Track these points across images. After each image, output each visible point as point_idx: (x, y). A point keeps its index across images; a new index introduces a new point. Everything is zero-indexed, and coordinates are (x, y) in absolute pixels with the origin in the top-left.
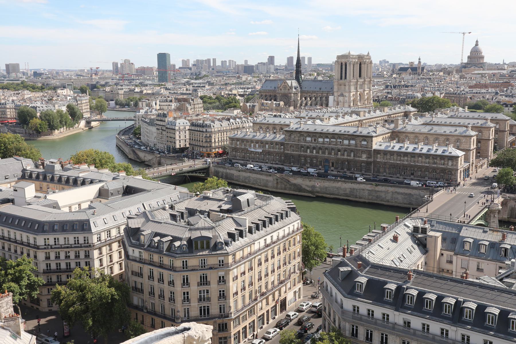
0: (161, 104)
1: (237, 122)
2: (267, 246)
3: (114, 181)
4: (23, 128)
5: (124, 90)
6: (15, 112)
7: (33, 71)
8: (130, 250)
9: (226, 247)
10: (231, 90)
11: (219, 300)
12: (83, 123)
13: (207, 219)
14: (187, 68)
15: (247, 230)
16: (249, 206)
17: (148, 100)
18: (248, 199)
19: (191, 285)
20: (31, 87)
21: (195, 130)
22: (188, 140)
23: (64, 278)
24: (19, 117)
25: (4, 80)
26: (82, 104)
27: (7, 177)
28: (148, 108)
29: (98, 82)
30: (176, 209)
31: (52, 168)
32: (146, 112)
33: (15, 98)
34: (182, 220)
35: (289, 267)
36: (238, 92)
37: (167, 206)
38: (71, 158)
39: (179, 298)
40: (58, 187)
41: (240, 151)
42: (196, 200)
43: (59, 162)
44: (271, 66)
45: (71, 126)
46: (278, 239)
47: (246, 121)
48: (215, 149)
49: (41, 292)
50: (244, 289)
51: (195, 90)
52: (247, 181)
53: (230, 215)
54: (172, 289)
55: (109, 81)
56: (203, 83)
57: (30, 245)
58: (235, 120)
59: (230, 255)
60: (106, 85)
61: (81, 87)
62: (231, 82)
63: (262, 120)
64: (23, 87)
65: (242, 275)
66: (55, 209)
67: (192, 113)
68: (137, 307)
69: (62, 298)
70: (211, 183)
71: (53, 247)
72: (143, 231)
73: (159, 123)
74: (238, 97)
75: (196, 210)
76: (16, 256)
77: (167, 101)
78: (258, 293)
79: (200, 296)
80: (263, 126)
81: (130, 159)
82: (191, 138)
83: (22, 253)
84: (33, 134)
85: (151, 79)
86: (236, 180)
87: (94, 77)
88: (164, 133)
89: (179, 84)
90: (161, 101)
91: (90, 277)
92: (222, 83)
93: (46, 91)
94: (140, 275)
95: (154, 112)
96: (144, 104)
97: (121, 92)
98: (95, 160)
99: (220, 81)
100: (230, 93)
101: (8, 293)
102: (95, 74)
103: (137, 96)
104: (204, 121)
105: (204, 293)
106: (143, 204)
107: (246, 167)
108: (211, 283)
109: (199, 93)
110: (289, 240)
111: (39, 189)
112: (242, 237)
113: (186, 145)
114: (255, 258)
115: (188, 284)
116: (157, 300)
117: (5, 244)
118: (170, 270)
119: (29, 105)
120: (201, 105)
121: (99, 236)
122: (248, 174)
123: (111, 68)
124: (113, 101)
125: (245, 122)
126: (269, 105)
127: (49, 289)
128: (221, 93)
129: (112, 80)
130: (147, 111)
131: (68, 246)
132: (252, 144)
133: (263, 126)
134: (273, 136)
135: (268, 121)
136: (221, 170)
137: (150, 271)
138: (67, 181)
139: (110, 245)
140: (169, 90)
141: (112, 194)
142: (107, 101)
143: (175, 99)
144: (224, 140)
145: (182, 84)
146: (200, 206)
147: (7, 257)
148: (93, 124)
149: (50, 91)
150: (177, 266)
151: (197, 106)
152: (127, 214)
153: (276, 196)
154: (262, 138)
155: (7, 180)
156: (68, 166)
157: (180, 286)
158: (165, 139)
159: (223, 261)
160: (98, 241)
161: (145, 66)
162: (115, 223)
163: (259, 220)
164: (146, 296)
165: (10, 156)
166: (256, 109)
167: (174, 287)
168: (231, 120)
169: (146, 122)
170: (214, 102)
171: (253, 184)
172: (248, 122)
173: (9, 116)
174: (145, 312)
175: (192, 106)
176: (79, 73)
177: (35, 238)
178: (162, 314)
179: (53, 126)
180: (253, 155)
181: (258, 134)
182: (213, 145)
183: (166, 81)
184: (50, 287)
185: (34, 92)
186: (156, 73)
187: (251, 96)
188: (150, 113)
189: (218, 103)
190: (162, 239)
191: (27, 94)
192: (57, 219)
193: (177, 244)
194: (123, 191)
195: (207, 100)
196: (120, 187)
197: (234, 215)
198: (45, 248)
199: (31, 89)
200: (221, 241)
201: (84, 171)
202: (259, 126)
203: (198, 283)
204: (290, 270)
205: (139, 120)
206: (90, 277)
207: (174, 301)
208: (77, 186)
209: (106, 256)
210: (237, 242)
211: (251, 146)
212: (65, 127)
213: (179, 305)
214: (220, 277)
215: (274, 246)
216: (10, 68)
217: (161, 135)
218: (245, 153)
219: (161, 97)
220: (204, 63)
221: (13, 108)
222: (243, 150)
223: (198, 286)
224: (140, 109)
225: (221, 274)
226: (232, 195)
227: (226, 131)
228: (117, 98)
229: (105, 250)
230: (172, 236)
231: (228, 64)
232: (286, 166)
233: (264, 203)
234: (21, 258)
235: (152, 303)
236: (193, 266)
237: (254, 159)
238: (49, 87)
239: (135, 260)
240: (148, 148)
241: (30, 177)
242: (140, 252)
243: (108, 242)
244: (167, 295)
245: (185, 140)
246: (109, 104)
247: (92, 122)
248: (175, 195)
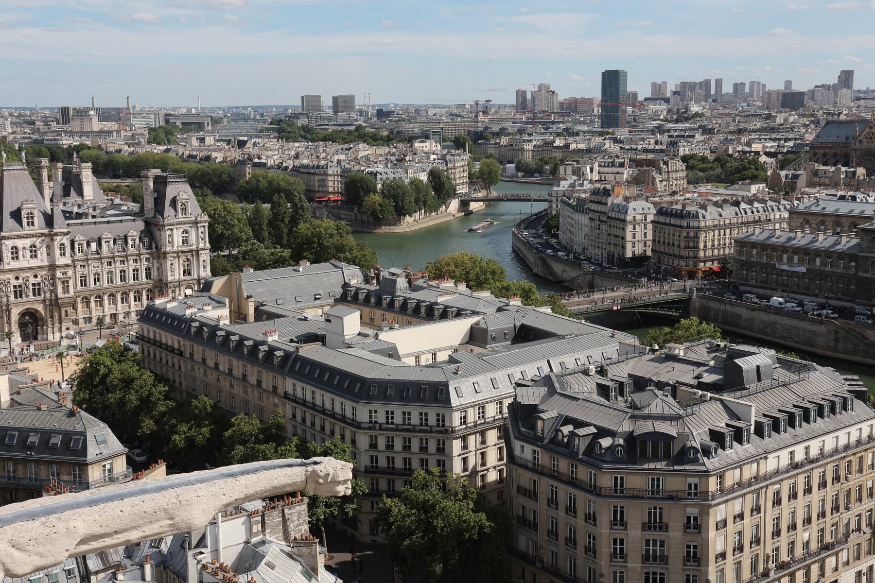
1: (754, 209)
2: (795, 466)
3: (499, 314)
4: (352, 210)
5: (534, 142)
6: (341, 182)
7: (377, 108)
8: (517, 445)
9: (705, 459)
10: (749, 144)
11: (684, 565)
12: (454, 204)
13: (670, 399)
14: (660, 99)
15: (753, 428)
16: (759, 379)
18: (758, 367)
19: (629, 527)
20: (371, 137)
21: (665, 224)
22: (650, 243)
23: (399, 486)
24: (346, 190)
25: (328, 125)
26: (455, 168)
27: (317, 297)
28: (575, 177)
29: (486, 128)
30: (609, 375)
31: (389, 285)
32: (572, 185)
33: (342, 157)
34: (620, 398)
35: (845, 516)
36: (764, 147)
37: (592, 368)
38: (427, 268)
39: (605, 549)
40: (400, 320)
41: (758, 269)
42: (652, 360)
43: (405, 274)
44: (844, 91)
45: (435, 208)
46: (821, 453)
47: (775, 208)
48: (705, 262)
49: (361, 507)
50: (740, 548)
51: (674, 144)
52: (769, 330)
53: (717, 396)
54: (591, 529)
55: (509, 125)
56: (691, 130)
57: (346, 419)
58: (752, 204)
59: (713, 475)
60: (502, 132)
61: (455, 137)
62: (751, 126)
63: (810, 207)
64: (358, 137)
65: (738, 519)
66: (391, 360)
67: (663, 189)
68: (523, 556)
69: (392, 520)
70: (688, 329)
71: (384, 426)
72: (543, 412)
73: (594, 207)
74: (763, 159)
75: (650, 380)
76: (324, 436)
77: (613, 164)
78: (770, 562)
79: (647, 551)
80: (810, 219)
81: (536, 275)
82: (657, 239)
83: (333, 433)
84: (368, 221)
85: (588, 121)
86: (746, 328)
87: (481, 117)
89: (642, 131)
90: (603, 164)
91: (444, 489)
92: (732, 128)
93: (395, 145)
94: (533, 495)
95: (587, 186)
96: (569, 170)
97: (529, 147)
98: (468, 273)
99: (728, 124)
100: (747, 149)
101: (300, 498)
102: (484, 113)
103: (558, 155)
104: (684, 206)
105: (655, 545)
106: (548, 362)
107: (769, 301)
108: (670, 528)
109: (681, 150)
110: (847, 460)
111: (368, 320)
112: (740, 442)
113: (645, 251)
114: (767, 487)
115: (624, 524)
116: (561, 548)
117: (326, 422)
118: (590, 492)
119: (365, 170)
120: (682, 174)
121: (463, 414)
122: (773, 317)
123: (512, 100)
124: (512, 163)
125: (773, 210)
126: (830, 175)
127: (372, 503)
128: (727, 150)
129: (514, 123)
130: (574, 183)
131: (409, 427)
132: (785, 256)
133: (810, 219)
134: (832, 240)
135: (824, 208)
136: (714, 305)
137: (552, 490)
138: (417, 310)
139: (483, 433)
140: (621, 142)
141: (493, 339)
142: (502, 163)
143: (630, 160)
144: (725, 244)
145: (648, 131)
146: (657, 373)
147: (309, 437)
148: (474, 206)
149: (401, 145)
150: (604, 486)
151: (674, 175)
152: (518, 377)
153: (824, 365)
154: (808, 244)
155: (317, 302)
156: (420, 282)
157: (608, 525)
159: (696, 486)
160: (461, 423)
161: (578, 96)
162: (495, 393)
163: (780, 411)
164: (542, 537)
165: (326, 260)
166: (802, 182)
167: (595, 525)
168: (743, 206)
169: (569, 205)
170: (711, 168)
171: (781, 337)
172: (779, 209)
173: (331, 189)
174: (539, 568)
175: (665, 176)
176: (455, 111)
177: (354, 409)
178: (571, 575)
179: (403, 207)
180: (785, 278)
181: (799, 234)
182: (701, 254)
183: (617, 126)
184: (375, 499)
185: (374, 146)
186: (597, 110)
187: (791, 156)
188: (579, 188)
189: (719, 170)
190: (576, 431)
191: (364, 150)
192: (391, 378)
193: (606, 442)
194: (513, 334)
195: (695, 162)
196: (509, 326)
197: (726, 397)
198: (370, 428)
199: (371, 140)
200: (694, 445)
201: (446, 293)
202: (802, 219)
203: (644, 524)
204: (848, 524)
205: (557, 201)
206: (444, 489)
207: (595, 553)
208: (433, 320)
209: (474, 453)
210: (729, 451)
211: (782, 259)
212: (423, 211)
213: (603, 563)
214: (689, 518)
215: (812, 469)
216: (340, 104)
217: (597, 231)
218: (767, 274)
219: (604, 158)
220: (698, 90)
221: (338, 175)
222: (764, 266)
223: (643, 530)
225: (693, 511)
226: (725, 356)
227: (731, 226)
228: (520, 157)
229: (473, 441)
230: (596, 427)
231: (747, 90)
232: (860, 304)
233: (795, 377)
234: (332, 443)
235: (552, 552)
236: (634, 490)
237: (787, 286)
238: (400, 136)
239: (524, 466)
240: (571, 256)
241: (355, 299)
242: (535, 451)
243: (479, 428)
244: (582, 540)
245: (645, 243)
246: (504, 170)
247: (471, 203)
248: (612, 347)
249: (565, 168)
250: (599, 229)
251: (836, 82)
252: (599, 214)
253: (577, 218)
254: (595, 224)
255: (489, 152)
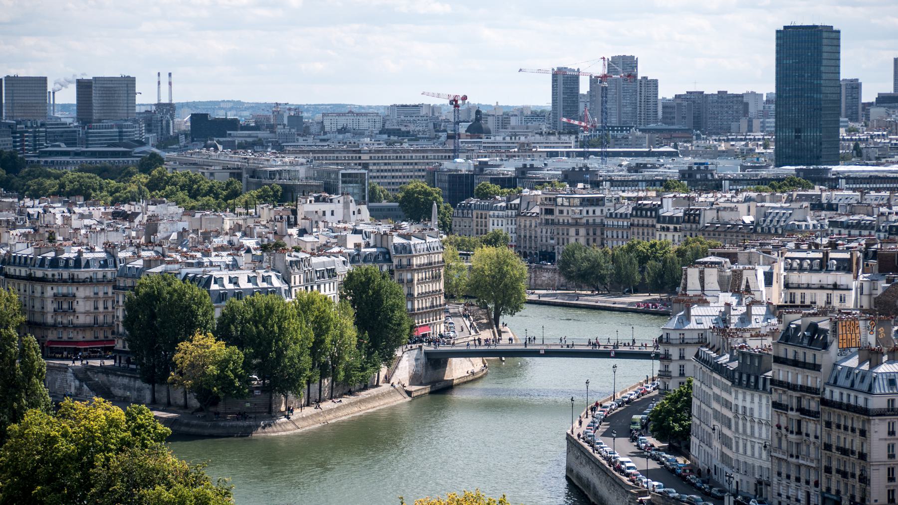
0: (795, 278)
17: (733, 257)
77: (823, 265)
88: (810, 426)
96: (712, 276)
158: (812, 456)
169: (719, 369)
217: (793, 437)
224: (688, 304)
249: (702, 273)
250: (799, 433)
251: (666, 92)
252: (796, 394)
253: (740, 403)
254: (790, 419)
255: (491, 229)
